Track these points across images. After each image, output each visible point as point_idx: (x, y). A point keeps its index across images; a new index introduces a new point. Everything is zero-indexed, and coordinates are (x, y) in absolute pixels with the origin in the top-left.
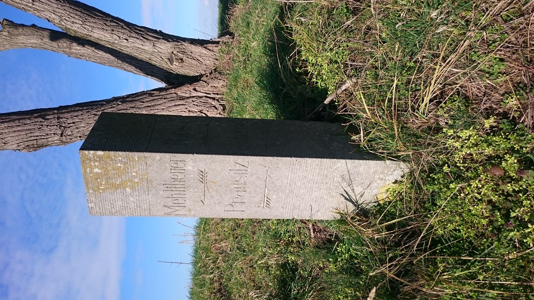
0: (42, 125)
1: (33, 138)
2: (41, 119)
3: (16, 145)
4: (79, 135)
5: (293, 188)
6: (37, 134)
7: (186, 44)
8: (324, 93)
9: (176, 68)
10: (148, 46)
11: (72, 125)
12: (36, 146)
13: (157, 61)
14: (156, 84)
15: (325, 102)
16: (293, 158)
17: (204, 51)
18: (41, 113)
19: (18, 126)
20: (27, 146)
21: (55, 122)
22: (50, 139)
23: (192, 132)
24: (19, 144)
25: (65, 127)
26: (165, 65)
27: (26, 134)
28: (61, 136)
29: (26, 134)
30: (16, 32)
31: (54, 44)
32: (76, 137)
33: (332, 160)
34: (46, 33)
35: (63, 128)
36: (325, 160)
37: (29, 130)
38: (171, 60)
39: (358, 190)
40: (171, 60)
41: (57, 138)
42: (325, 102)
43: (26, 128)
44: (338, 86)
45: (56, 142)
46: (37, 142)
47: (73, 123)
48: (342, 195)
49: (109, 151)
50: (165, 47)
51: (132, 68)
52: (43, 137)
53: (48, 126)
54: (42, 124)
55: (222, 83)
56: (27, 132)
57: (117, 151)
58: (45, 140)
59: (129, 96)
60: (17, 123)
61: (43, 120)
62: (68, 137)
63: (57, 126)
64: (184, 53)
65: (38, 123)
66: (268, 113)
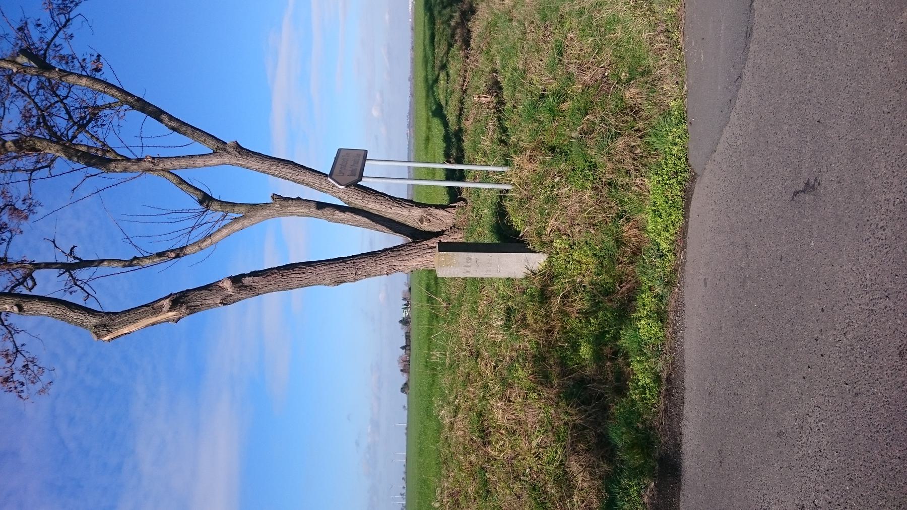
7: (432, 209)
8: (520, 232)
9: (425, 227)
10: (405, 212)
13: (410, 223)
14: (398, 240)
17: (446, 213)
18: (343, 260)
21: (352, 265)
26: (416, 224)
30: (286, 204)
31: (320, 212)
34: (312, 204)
38: (421, 221)
39: (531, 265)
40: (421, 221)
41: (352, 276)
44: (525, 230)
50: (417, 212)
51: (384, 229)
55: (460, 235)
59: (395, 247)
60: (331, 266)
64: (431, 215)
66: (495, 241)
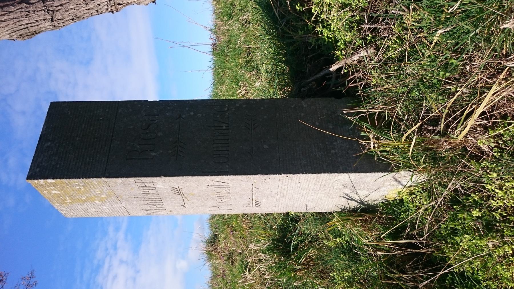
0: (28, 12)
1: (23, 27)
2: (25, 5)
3: (8, 36)
4: (71, 18)
5: (285, 194)
6: (26, 22)
11: (60, 8)
12: (29, 34)
15: (331, 69)
16: (283, 175)
19: (4, 15)
20: (21, 35)
22: (41, 26)
23: (160, 134)
24: (11, 35)
25: (53, 11)
27: (15, 23)
28: (52, 21)
29: (15, 23)
32: (68, 20)
33: (332, 174)
35: (51, 12)
36: (323, 175)
37: (16, 18)
41: (48, 24)
42: (331, 69)
43: (12, 17)
45: (48, 27)
46: (29, 30)
47: (61, 5)
48: (343, 197)
49: (60, 178)
52: (33, 25)
53: (34, 11)
54: (28, 10)
56: (15, 21)
57: (70, 178)
58: (36, 27)
61: (28, 6)
62: (60, 21)
63: (45, 11)
65: (23, 10)
